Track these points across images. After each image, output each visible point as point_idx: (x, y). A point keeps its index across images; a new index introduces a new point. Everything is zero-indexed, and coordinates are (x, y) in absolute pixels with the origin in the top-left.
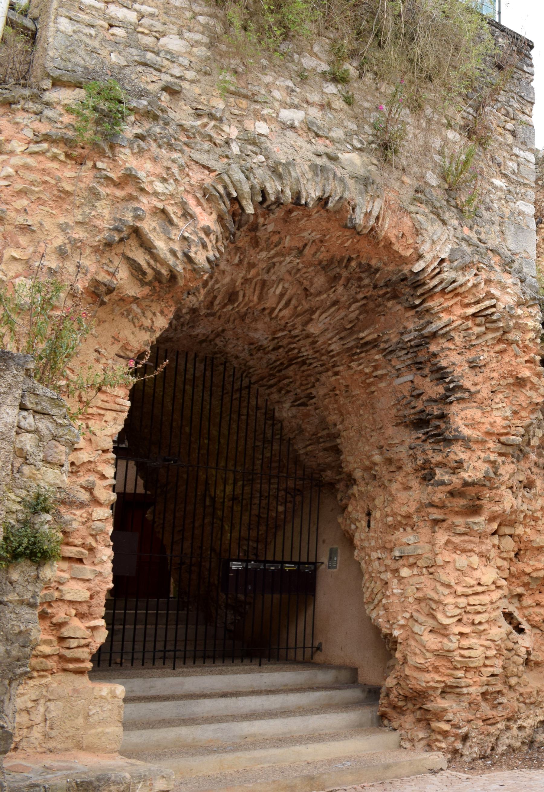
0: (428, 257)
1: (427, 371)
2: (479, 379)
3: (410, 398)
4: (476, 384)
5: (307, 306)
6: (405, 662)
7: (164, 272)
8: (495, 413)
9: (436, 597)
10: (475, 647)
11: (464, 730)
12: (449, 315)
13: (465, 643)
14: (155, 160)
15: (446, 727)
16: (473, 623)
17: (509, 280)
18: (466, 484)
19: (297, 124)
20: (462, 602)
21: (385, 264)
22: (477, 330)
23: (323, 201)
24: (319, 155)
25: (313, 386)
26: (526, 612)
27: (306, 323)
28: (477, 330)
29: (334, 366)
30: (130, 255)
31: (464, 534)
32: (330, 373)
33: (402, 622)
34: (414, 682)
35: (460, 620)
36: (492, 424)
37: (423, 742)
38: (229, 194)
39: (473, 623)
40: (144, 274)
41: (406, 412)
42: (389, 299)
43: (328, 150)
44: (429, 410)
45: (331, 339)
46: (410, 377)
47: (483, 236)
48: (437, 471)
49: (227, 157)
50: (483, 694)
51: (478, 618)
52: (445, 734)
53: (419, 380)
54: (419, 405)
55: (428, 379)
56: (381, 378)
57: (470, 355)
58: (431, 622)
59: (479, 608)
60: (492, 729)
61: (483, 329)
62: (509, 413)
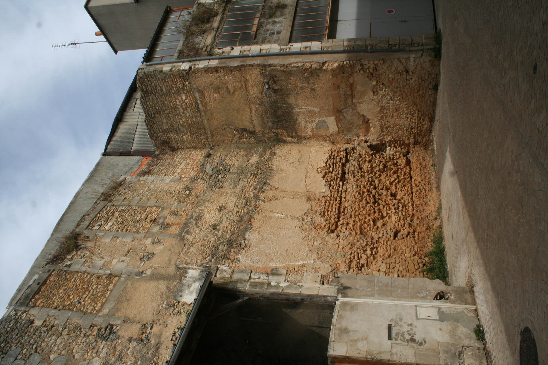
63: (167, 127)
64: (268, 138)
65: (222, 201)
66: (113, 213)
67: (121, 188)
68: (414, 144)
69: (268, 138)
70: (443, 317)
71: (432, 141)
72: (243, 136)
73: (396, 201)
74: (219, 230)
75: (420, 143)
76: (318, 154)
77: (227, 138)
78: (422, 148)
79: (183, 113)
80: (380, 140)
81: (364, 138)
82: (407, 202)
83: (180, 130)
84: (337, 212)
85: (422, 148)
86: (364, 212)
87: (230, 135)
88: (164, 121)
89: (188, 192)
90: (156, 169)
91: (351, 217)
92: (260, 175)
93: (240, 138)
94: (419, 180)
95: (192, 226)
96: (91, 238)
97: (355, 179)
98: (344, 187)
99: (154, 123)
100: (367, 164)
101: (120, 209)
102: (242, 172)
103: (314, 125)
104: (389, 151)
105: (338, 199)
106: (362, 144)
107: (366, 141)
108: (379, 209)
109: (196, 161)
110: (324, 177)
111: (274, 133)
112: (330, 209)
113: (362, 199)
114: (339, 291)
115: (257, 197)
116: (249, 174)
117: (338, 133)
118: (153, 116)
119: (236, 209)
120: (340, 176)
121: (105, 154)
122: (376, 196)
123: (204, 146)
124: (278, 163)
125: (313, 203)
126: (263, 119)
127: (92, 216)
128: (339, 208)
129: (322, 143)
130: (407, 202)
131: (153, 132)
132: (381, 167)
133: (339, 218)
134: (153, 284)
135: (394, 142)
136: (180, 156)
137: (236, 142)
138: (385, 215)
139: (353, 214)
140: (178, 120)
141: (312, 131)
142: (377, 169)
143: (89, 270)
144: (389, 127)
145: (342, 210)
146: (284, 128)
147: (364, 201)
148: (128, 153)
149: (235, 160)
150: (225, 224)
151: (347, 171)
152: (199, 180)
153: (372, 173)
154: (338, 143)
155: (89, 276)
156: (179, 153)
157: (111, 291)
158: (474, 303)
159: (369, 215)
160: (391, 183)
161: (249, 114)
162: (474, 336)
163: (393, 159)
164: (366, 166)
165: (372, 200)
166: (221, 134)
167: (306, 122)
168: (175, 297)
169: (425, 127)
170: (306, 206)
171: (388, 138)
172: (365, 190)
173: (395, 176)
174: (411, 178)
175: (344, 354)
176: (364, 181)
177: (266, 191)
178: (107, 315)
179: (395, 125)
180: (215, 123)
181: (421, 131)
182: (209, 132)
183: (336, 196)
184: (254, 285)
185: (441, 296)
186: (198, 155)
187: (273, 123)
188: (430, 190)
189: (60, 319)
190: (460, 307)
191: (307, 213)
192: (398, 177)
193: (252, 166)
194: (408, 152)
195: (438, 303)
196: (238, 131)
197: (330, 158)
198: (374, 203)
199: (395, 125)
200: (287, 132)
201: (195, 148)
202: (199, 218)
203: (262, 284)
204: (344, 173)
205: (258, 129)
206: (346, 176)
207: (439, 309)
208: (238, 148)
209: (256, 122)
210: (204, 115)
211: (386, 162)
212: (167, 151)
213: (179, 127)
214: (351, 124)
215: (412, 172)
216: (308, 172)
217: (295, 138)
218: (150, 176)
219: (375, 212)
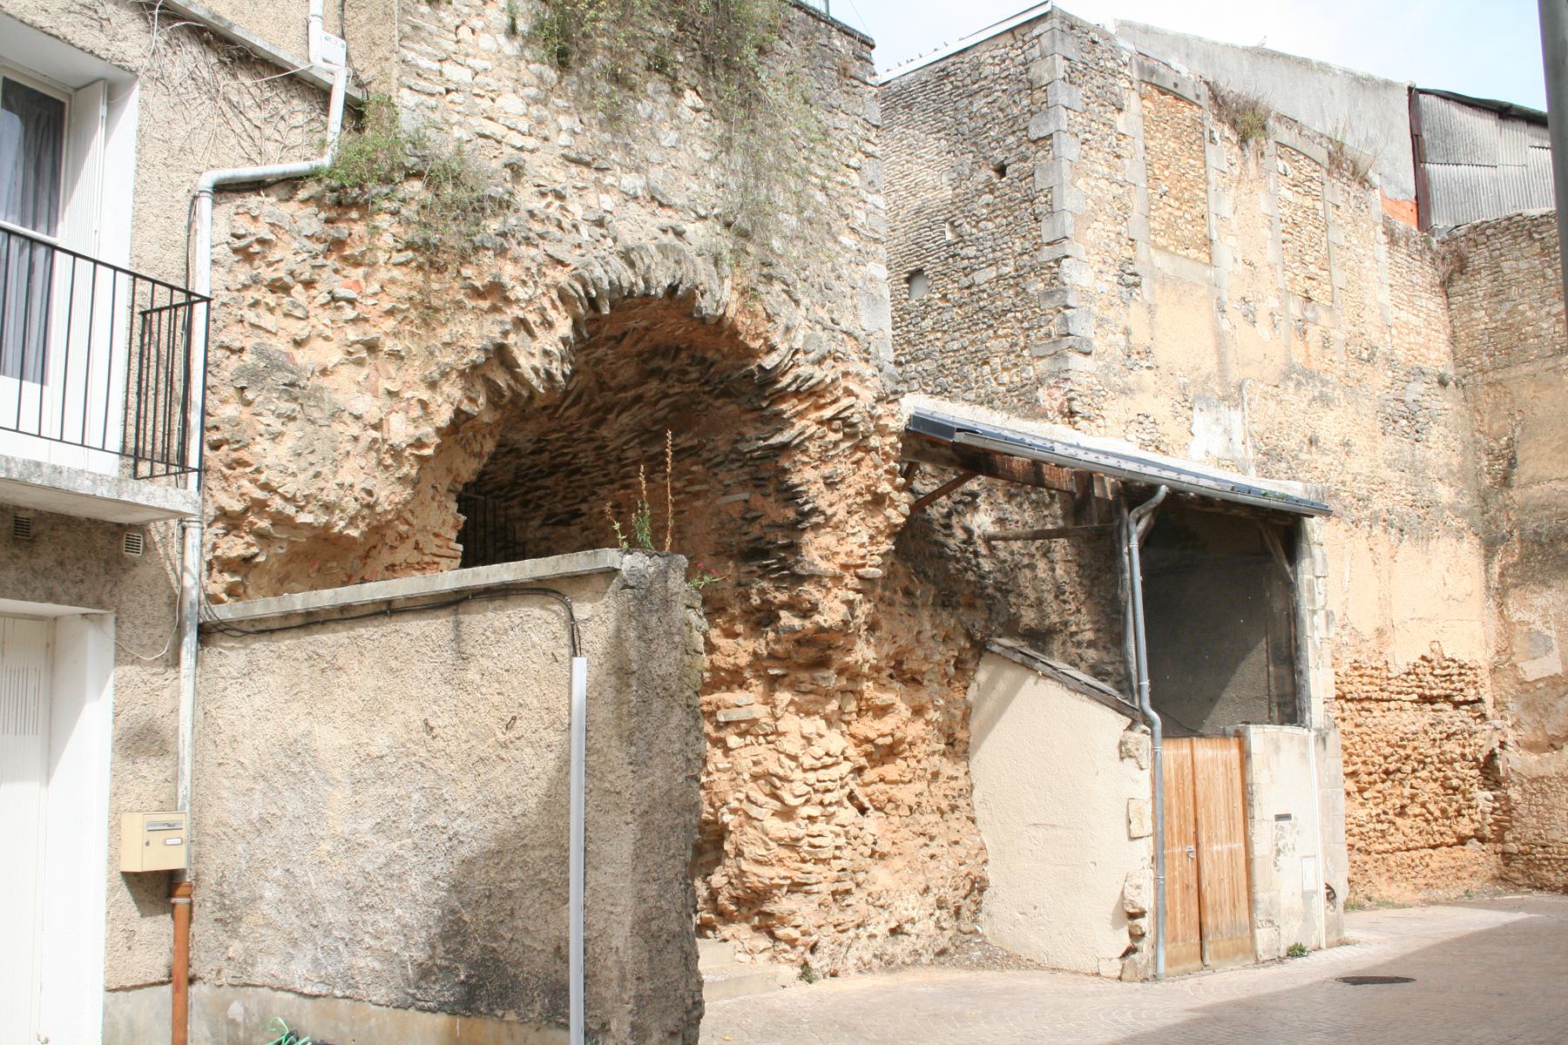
0: (783, 348)
1: (771, 488)
2: (834, 497)
3: (740, 522)
4: (831, 505)
5: (600, 402)
6: (739, 853)
7: (525, 393)
8: (852, 539)
9: (781, 772)
10: (826, 833)
11: (815, 938)
12: (804, 424)
13: (815, 829)
14: (516, 260)
15: (795, 934)
16: (821, 803)
17: (868, 371)
18: (821, 629)
19: (640, 193)
20: (811, 777)
21: (724, 356)
22: (832, 437)
23: (672, 289)
24: (665, 231)
25: (585, 500)
26: (869, 790)
27: (598, 424)
28: (832, 437)
29: (623, 478)
30: (491, 375)
31: (811, 692)
32: (617, 486)
33: (735, 804)
34: (754, 879)
35: (807, 801)
36: (849, 554)
37: (767, 954)
38: (587, 293)
39: (821, 803)
40: (502, 396)
41: (734, 540)
42: (717, 397)
43: (673, 223)
44: (771, 537)
45: (625, 443)
46: (745, 496)
47: (836, 316)
48: (783, 613)
49: (579, 246)
50: (834, 893)
51: (828, 798)
52: (792, 943)
53: (757, 500)
54: (755, 531)
55: (771, 499)
56: (697, 495)
57: (826, 470)
58: (776, 805)
59: (830, 785)
60: (843, 937)
61: (840, 435)
62: (866, 539)
63: (1507, 271)
64: (1494, 520)
65: (1360, 442)
66: (1307, 194)
67: (1356, 186)
68: (1503, 853)
69: (1494, 520)
70: (1307, 896)
71: (1517, 892)
72: (1497, 459)
73: (1391, 817)
74: (1310, 452)
75: (1507, 865)
76: (1468, 637)
77: (1487, 418)
78: (1495, 871)
79: (1548, 313)
80: (1507, 778)
81: (1510, 740)
82: (1391, 839)
83: (1501, 302)
84: (1363, 695)
85: (1495, 871)
86: (1369, 753)
87: (1495, 426)
88: (1523, 265)
89: (1365, 355)
90: (1401, 256)
91: (1357, 726)
92: (1414, 513)
93: (1490, 452)
94: (1434, 865)
95: (1311, 391)
96: (1261, 161)
97: (1428, 728)
98: (1407, 705)
99: (1515, 238)
100: (1459, 750)
101: (1319, 205)
102: (1415, 470)
103: (1538, 626)
104: (1483, 797)
105: (1385, 695)
106: (1497, 737)
107: (1502, 745)
108: (1375, 782)
109: (1424, 351)
110: (1423, 658)
111: (1511, 532)
112: (1365, 680)
113: (1391, 746)
114: (1319, 730)
115: (1374, 518)
116: (1415, 490)
117: (1522, 683)
118: (1536, 236)
119: (1349, 478)
120: (1427, 693)
121: (1413, 93)
122: (1399, 775)
123: (1459, 362)
124: (1444, 547)
125: (1373, 644)
126: (1544, 507)
127: (1300, 144)
128: (1369, 699)
129: (1493, 644)
130: (1391, 839)
131: (1489, 232)
132: (1455, 782)
133: (1352, 700)
134: (1208, 342)
135: (1506, 809)
136: (1432, 306)
137: (1476, 442)
138: (1366, 795)
139: (1364, 729)
140: (1527, 300)
141: (1521, 623)
142: (1450, 774)
143: (1211, 189)
144: (1545, 795)
145: (1366, 704)
146: (1525, 558)
147: (1388, 751)
148: (1419, 156)
149: (1442, 447)
150: (1322, 462)
151: (1437, 706)
152: (1390, 373)
153: (1441, 762)
154: (1495, 682)
155: (1202, 195)
156: (1439, 300)
157: (1187, 257)
158: (1330, 946)
159: (1364, 763)
160: (1423, 805)
161: (1557, 475)
162: (1292, 944)
163: (1470, 807)
164: (1453, 748)
165: (1392, 767)
166: (1497, 406)
167: (1546, 610)
168: (1198, 397)
169: (1551, 876)
170: (1368, 630)
171: (1514, 793)
172: (1409, 751)
173: (1437, 814)
174: (1434, 847)
175: (1253, 750)
176: (1425, 747)
177: (1386, 537)
178: (1152, 265)
179: (1550, 809)
180: (1527, 393)
181: (1540, 867)
182: (1499, 376)
183: (1391, 688)
184: (1311, 589)
185: (1331, 894)
186: (1438, 357)
187: (1536, 532)
188: (1417, 888)
189: (1132, 169)
190: (1321, 924)
191: (1355, 632)
192: (1436, 820)
193: (1432, 491)
194: (1482, 840)
195: (1323, 891)
196: (1508, 446)
197: (1461, 667)
198: (1387, 772)
199: (1550, 809)
200: (1515, 565)
201: (1454, 340)
202: (1325, 400)
203: (1313, 601)
204: (1431, 700)
205: (1516, 495)
206: (1428, 707)
207: (1315, 892)
208: (1465, 448)
209: (1535, 490)
210: (1546, 366)
211: (1463, 793)
212: (1441, 268)
213: (1507, 300)
214: (1546, 709)
215: (1444, 848)
216: (1430, 621)
217: (1501, 582)
218: (1385, 248)
219: (1370, 774)
